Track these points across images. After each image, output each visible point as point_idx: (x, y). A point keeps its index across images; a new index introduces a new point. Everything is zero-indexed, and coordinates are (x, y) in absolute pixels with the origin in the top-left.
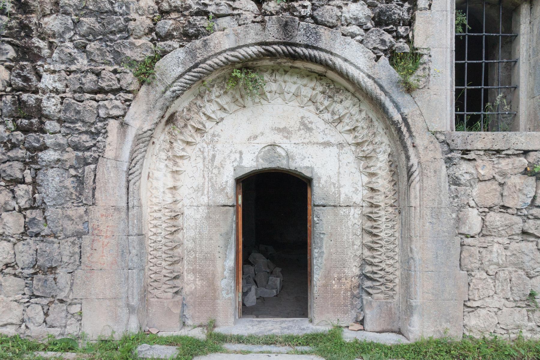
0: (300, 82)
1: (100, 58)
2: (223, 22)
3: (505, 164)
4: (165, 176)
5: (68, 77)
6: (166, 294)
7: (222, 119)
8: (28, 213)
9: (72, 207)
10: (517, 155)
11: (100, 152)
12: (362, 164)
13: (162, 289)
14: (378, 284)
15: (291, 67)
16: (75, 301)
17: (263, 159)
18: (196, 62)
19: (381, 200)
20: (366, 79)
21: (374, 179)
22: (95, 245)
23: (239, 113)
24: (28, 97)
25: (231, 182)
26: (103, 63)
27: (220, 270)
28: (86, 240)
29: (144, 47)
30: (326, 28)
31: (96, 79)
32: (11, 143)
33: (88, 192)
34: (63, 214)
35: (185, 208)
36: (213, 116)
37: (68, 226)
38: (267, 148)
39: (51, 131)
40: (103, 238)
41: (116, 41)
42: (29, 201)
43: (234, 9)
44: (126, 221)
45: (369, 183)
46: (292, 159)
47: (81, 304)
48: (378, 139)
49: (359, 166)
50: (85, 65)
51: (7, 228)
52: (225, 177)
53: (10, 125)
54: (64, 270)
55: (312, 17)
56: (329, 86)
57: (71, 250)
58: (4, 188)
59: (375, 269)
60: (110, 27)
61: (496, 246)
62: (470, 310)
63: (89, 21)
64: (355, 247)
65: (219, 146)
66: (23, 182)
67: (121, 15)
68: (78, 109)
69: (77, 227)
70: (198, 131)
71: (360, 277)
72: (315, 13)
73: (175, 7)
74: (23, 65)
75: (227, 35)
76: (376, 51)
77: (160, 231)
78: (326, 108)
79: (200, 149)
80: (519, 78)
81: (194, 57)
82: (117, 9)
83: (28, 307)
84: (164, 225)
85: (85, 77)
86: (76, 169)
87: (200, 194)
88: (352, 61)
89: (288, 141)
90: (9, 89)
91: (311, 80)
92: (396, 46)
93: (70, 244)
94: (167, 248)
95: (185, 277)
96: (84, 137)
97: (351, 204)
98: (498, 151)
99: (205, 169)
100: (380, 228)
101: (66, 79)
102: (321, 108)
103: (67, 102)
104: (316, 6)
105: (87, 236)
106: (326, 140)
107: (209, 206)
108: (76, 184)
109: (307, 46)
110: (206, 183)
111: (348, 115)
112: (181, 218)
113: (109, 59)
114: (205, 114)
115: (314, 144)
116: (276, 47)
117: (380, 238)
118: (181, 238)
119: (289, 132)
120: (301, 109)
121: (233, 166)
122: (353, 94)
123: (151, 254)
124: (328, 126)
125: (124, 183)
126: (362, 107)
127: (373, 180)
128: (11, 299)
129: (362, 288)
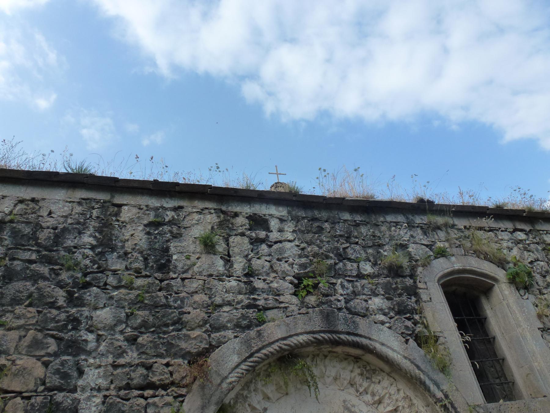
1: (153, 350)
2: (270, 314)
5: (115, 373)
15: (330, 352)
18: (252, 351)
20: (405, 361)
24: (64, 397)
26: (154, 356)
29: (199, 339)
30: (360, 317)
31: (147, 373)
41: (170, 333)
43: (282, 302)
50: (135, 359)
56: (365, 368)
60: (165, 319)
63: (142, 315)
67: (175, 308)
68: (122, 409)
72: (348, 305)
73: (228, 301)
74: (65, 360)
75: (279, 326)
76: (404, 335)
78: (365, 390)
81: (249, 346)
82: (172, 303)
88: (389, 345)
90: (41, 388)
91: (349, 363)
92: (417, 330)
101: (112, 374)
102: (361, 390)
103: (111, 401)
104: (348, 300)
109: (349, 333)
111: (387, 395)
114: (249, 405)
116: (322, 335)
120: (341, 392)
122: (388, 374)
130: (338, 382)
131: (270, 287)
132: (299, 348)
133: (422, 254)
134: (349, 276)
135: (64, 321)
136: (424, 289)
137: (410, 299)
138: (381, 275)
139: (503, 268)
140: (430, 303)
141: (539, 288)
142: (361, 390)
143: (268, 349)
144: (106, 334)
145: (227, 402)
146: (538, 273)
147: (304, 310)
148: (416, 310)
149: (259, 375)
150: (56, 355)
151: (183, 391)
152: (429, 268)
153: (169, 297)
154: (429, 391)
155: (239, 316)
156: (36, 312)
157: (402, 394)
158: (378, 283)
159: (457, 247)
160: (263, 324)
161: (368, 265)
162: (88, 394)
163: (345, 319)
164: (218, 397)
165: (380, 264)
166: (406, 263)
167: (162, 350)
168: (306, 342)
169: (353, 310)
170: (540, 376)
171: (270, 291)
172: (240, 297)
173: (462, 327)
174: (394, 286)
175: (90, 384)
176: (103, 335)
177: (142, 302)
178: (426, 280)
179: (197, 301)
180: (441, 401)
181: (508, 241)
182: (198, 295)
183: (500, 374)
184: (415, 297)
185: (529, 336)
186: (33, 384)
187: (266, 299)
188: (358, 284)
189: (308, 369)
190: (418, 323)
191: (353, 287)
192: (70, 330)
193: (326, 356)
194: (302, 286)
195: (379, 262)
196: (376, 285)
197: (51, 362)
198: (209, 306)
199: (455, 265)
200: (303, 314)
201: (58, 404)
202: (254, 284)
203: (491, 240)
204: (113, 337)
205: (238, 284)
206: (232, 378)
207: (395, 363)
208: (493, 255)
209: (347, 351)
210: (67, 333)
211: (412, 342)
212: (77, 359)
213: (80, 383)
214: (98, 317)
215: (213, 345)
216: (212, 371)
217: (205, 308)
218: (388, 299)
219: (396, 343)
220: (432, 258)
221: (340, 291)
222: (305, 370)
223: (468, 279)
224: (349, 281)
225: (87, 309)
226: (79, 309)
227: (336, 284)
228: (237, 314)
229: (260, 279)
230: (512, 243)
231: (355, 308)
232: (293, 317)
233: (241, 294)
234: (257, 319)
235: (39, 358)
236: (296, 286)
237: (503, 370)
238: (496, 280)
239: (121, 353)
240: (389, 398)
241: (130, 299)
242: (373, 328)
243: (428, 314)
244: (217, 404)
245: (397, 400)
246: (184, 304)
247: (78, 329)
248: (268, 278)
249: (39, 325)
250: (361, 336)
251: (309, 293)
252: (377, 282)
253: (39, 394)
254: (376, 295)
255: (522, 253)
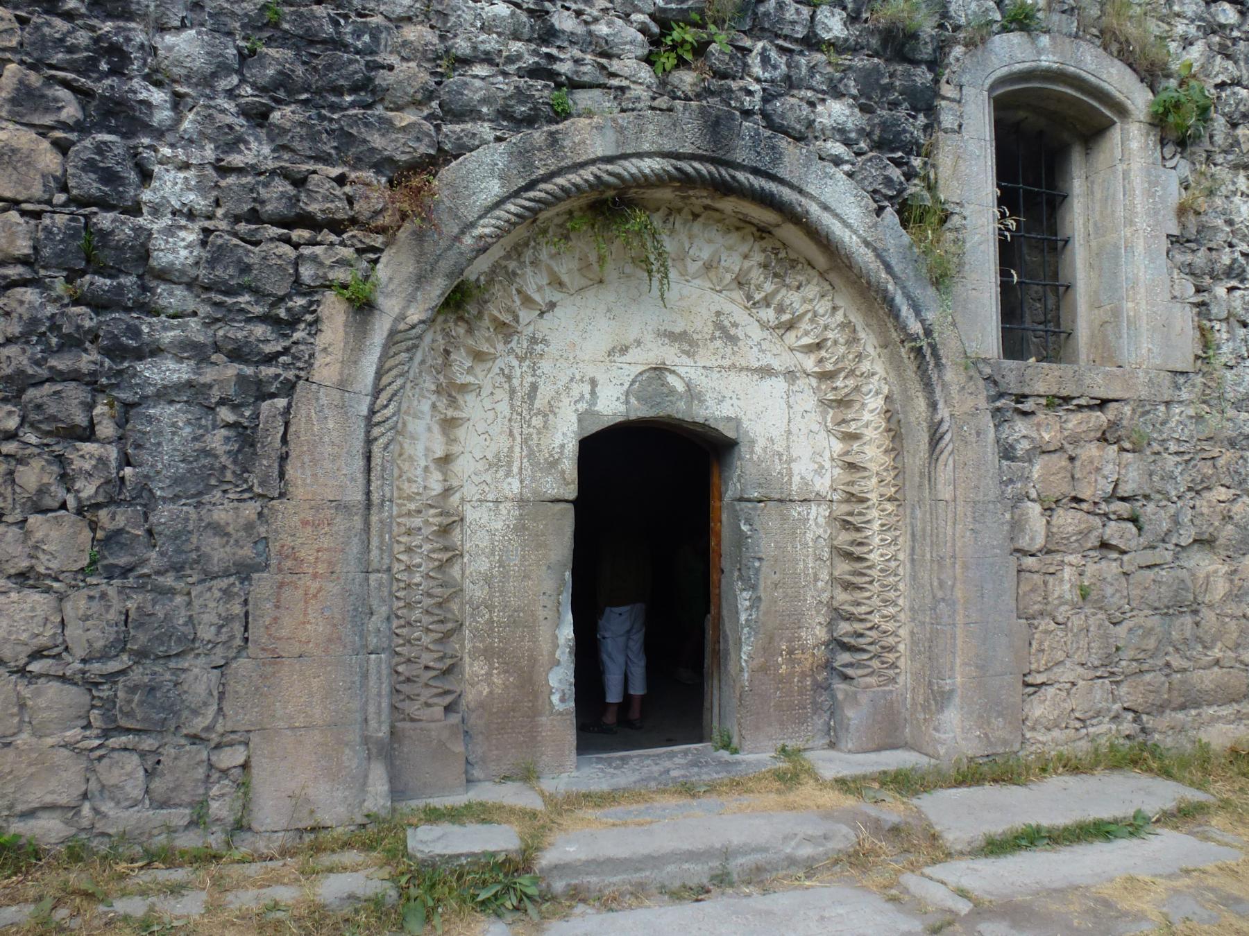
0: (720, 240)
1: (307, 144)
2: (584, 98)
3: (1075, 421)
4: (429, 429)
5: (223, 183)
6: (429, 711)
7: (552, 305)
8: (103, 514)
9: (226, 501)
10: (1090, 407)
11: (302, 369)
12: (831, 415)
13: (423, 699)
14: (865, 656)
15: (706, 208)
16: (233, 736)
17: (638, 399)
18: (534, 177)
19: (870, 488)
21: (856, 446)
22: (286, 593)
23: (590, 293)
24: (113, 221)
25: (572, 448)
26: (311, 157)
27: (545, 647)
28: (263, 584)
29: (414, 133)
31: (295, 192)
32: (60, 336)
33: (266, 463)
34: (201, 520)
35: (468, 507)
36: (537, 297)
37: (213, 549)
38: (645, 376)
39: (171, 311)
40: (308, 577)
41: (346, 109)
42: (108, 488)
44: (364, 537)
45: (847, 453)
46: (700, 401)
47: (247, 744)
48: (865, 366)
49: (825, 419)
50: (265, 158)
51: (41, 556)
52: (560, 434)
53: (60, 287)
54: (202, 660)
55: (765, 115)
56: (776, 254)
57: (221, 609)
58: (37, 451)
59: (858, 627)
60: (333, 75)
61: (1067, 569)
62: (1031, 690)
63: (277, 57)
64: (820, 584)
65: (545, 366)
66: (88, 434)
67: (358, 52)
69: (240, 552)
70: (499, 329)
71: (827, 646)
72: (768, 107)
73: (487, 53)
74: (105, 143)
75: (600, 128)
76: (877, 197)
77: (419, 560)
78: (765, 299)
79: (502, 369)
80: (1074, 269)
81: (529, 165)
82: (349, 39)
83: (100, 758)
84: (427, 547)
85: (266, 185)
86: (235, 407)
87: (501, 473)
88: (838, 211)
89: (690, 362)
91: (743, 239)
92: (909, 191)
93: (218, 594)
94: (431, 601)
95: (467, 669)
96: (260, 330)
97: (812, 496)
98: (1067, 399)
99: (515, 416)
100: (869, 545)
101: (217, 186)
102: (757, 297)
103: (220, 241)
105: (265, 575)
106: (763, 362)
107: (522, 501)
108: (236, 446)
109: (756, 171)
110: (517, 449)
111: (809, 315)
112: (458, 530)
113: (327, 148)
114: (519, 292)
115: (741, 370)
116: (697, 165)
117: (868, 564)
118: (458, 577)
119: (692, 343)
120: (715, 296)
121: (577, 410)
123: (398, 617)
124: (766, 334)
125: (358, 445)
126: (839, 302)
127: (855, 447)
128: (50, 741)
129: (833, 669)
130: (712, 274)
131: (590, 33)
132: (639, 186)
133: (975, 13)
134: (786, 38)
135: (87, 49)
136: (953, 100)
137: (914, 117)
138: (862, 48)
139: (1152, 88)
140: (956, 136)
141: (1210, 148)
142: (757, 297)
143: (570, 176)
144: (193, 94)
145: (473, 278)
146: (1224, 115)
147: (663, 102)
148: (919, 146)
149: (544, 232)
150: (81, 128)
151: (378, 241)
152: (979, 53)
153: (342, 22)
154: (897, 316)
155: (509, 93)
156: (13, 19)
157: (839, 316)
158: (850, 68)
159: (1064, 12)
160: (565, 119)
161: (837, 18)
162: (167, 221)
163: (756, 138)
164: (452, 262)
165: (866, 21)
166: (929, 30)
167: (329, 147)
168: (656, 175)
169: (778, 120)
170: (1128, 329)
171: (590, 43)
172: (516, 46)
173: (1006, 199)
174: (886, 81)
175: (168, 202)
176: (186, 95)
177: (276, 26)
178: (964, 80)
179: (412, 42)
180: (915, 340)
181: (1192, 21)
182: (413, 28)
183: (1049, 317)
184: (926, 116)
185: (1140, 248)
186: (41, 187)
187: (577, 61)
188: (803, 61)
189: (654, 235)
190: (916, 175)
191: (789, 66)
192: (107, 75)
193: (696, 216)
194: (668, 41)
195: (864, 16)
196: (843, 71)
197: (73, 143)
198: (441, 58)
199: (1043, 58)
200: (661, 110)
201: (104, 235)
202: (553, 20)
203: (1154, 10)
204: (212, 103)
205: (513, 14)
206: (485, 228)
207: (843, 252)
208: (1142, 50)
209: (744, 211)
210: (99, 80)
211: (890, 216)
212: (132, 143)
213: (146, 195)
214: (170, 49)
215: (446, 152)
216: (442, 207)
217: (429, 60)
218: (864, 109)
219: (857, 210)
220: (996, 27)
221: (757, 70)
222: (646, 236)
223: (1061, 97)
224: (782, 50)
225: (141, 27)
226: (121, 24)
227: (750, 51)
228: (505, 87)
229: (568, 9)
230: (1199, 27)
231: (783, 116)
232: (635, 113)
233: (519, 40)
234: (552, 106)
235: (43, 131)
236: (655, 41)
237: (1058, 308)
238: (1122, 111)
239: (236, 143)
240: (812, 321)
241: (246, 15)
242: (813, 168)
243: (945, 160)
244: (449, 276)
245: (826, 327)
246: (378, 45)
247: (125, 75)
248: (588, 10)
249: (28, 54)
250: (782, 181)
251: (682, 63)
252: (847, 62)
253: (58, 210)
254: (839, 95)
255: (1210, 60)
